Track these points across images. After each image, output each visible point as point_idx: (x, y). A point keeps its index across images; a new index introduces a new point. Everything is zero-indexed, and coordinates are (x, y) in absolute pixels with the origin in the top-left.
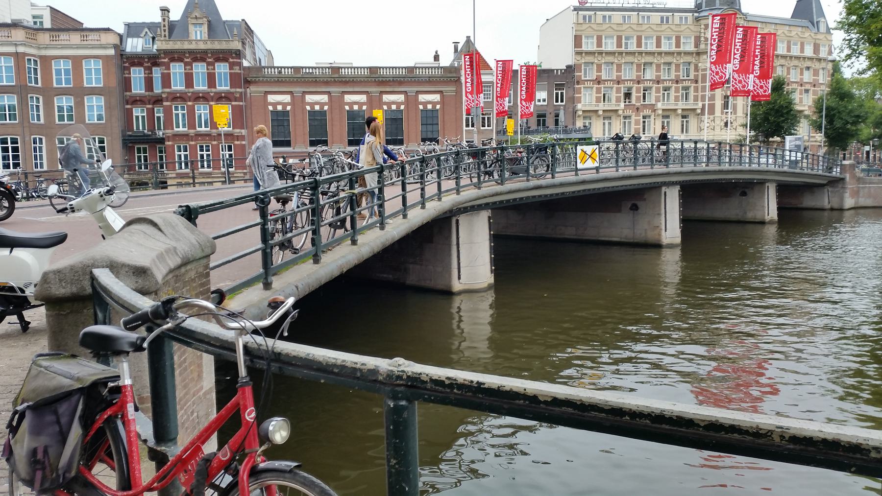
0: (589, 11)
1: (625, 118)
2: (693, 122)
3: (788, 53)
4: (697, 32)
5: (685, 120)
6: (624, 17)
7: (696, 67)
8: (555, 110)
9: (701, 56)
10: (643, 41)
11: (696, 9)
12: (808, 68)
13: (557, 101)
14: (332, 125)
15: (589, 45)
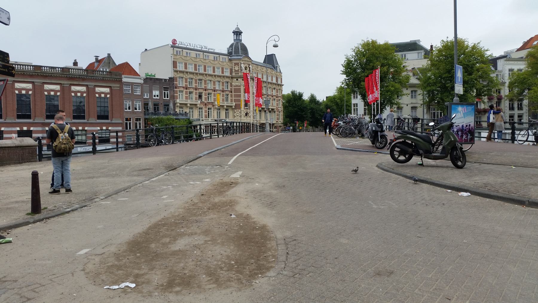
0: (179, 48)
1: (199, 109)
2: (231, 113)
3: (195, 71)
4: (231, 66)
5: (227, 111)
6: (196, 54)
7: (231, 84)
8: (164, 102)
9: (233, 79)
10: (207, 68)
11: (229, 54)
12: (274, 88)
13: (165, 97)
14: (35, 105)
15: (180, 67)
